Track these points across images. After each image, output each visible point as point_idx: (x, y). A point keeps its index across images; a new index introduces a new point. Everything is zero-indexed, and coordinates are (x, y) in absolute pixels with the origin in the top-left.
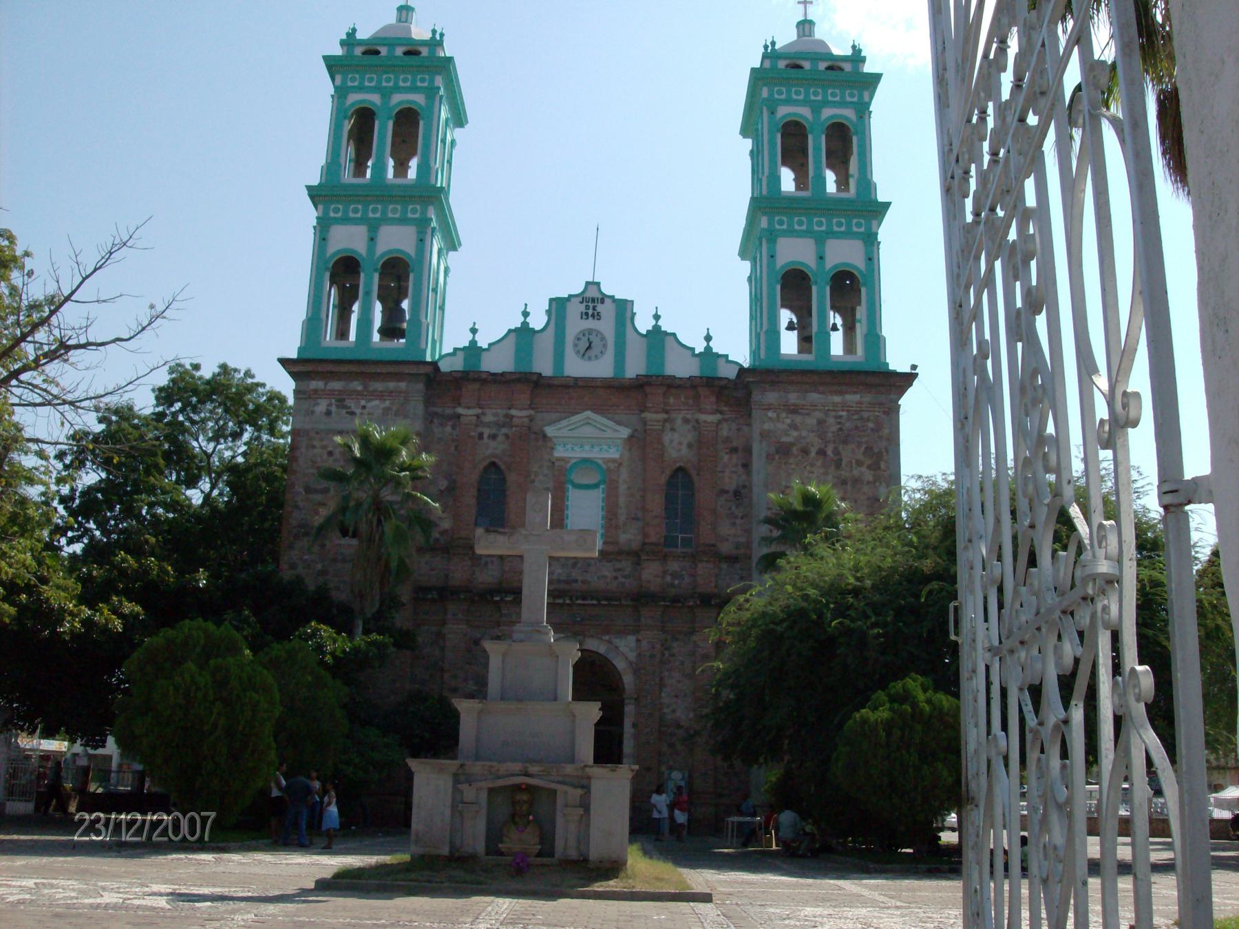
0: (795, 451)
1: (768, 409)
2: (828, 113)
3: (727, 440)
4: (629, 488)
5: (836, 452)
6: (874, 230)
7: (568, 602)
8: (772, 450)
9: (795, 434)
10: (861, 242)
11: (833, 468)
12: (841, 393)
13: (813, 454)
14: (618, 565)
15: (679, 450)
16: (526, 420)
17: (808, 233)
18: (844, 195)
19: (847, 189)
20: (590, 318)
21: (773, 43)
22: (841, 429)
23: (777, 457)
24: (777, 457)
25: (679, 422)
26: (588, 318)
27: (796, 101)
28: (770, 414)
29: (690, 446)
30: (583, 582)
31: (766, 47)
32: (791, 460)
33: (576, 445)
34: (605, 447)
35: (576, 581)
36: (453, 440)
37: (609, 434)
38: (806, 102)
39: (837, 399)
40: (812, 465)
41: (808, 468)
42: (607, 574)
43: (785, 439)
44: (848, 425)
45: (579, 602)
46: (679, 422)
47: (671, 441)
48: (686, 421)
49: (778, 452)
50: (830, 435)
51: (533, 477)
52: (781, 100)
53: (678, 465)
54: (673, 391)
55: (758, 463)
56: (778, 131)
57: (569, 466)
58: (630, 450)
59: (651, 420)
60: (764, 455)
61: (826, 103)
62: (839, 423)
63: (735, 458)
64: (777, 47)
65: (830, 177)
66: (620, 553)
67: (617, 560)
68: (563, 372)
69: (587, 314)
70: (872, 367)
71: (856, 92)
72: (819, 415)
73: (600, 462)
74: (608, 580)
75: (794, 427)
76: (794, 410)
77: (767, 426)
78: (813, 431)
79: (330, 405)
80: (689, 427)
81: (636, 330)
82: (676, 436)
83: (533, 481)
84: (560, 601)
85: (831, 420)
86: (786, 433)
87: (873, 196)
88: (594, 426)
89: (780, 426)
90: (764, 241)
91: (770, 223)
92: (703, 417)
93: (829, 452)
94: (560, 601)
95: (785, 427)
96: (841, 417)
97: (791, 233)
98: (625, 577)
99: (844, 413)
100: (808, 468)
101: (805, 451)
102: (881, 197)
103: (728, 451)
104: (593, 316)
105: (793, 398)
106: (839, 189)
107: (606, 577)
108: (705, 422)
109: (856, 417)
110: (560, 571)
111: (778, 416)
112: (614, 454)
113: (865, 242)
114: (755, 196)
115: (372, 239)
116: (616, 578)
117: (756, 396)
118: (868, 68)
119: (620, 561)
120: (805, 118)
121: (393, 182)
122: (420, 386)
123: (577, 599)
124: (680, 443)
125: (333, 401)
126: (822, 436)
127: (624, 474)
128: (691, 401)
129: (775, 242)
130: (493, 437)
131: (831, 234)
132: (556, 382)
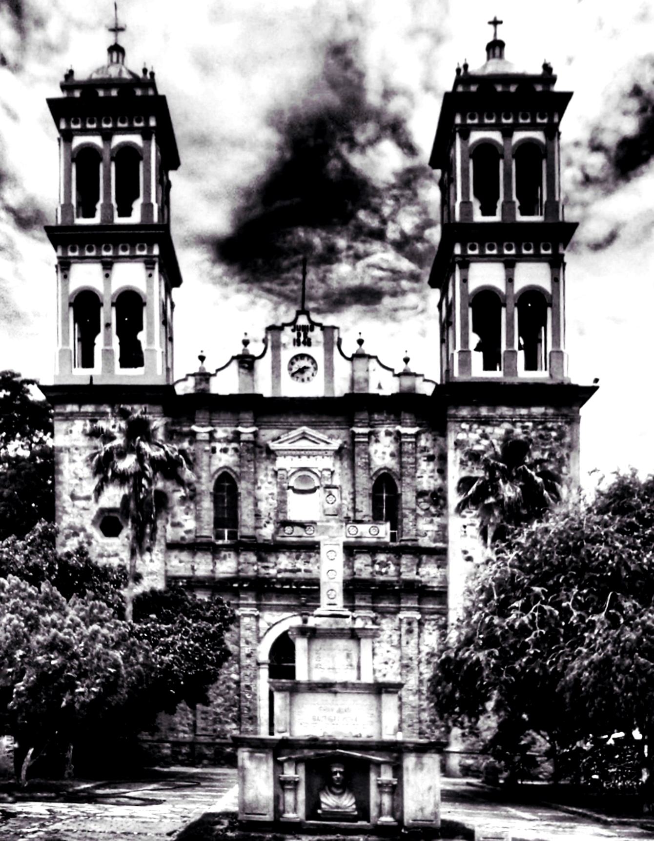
1: (462, 422)
30: (306, 571)
35: (299, 570)
37: (322, 446)
39: (524, 412)
43: (477, 448)
60: (458, 461)
75: (485, 436)
86: (478, 442)
88: (310, 440)
96: (527, 427)
99: (530, 424)
109: (540, 427)
118: (558, 88)
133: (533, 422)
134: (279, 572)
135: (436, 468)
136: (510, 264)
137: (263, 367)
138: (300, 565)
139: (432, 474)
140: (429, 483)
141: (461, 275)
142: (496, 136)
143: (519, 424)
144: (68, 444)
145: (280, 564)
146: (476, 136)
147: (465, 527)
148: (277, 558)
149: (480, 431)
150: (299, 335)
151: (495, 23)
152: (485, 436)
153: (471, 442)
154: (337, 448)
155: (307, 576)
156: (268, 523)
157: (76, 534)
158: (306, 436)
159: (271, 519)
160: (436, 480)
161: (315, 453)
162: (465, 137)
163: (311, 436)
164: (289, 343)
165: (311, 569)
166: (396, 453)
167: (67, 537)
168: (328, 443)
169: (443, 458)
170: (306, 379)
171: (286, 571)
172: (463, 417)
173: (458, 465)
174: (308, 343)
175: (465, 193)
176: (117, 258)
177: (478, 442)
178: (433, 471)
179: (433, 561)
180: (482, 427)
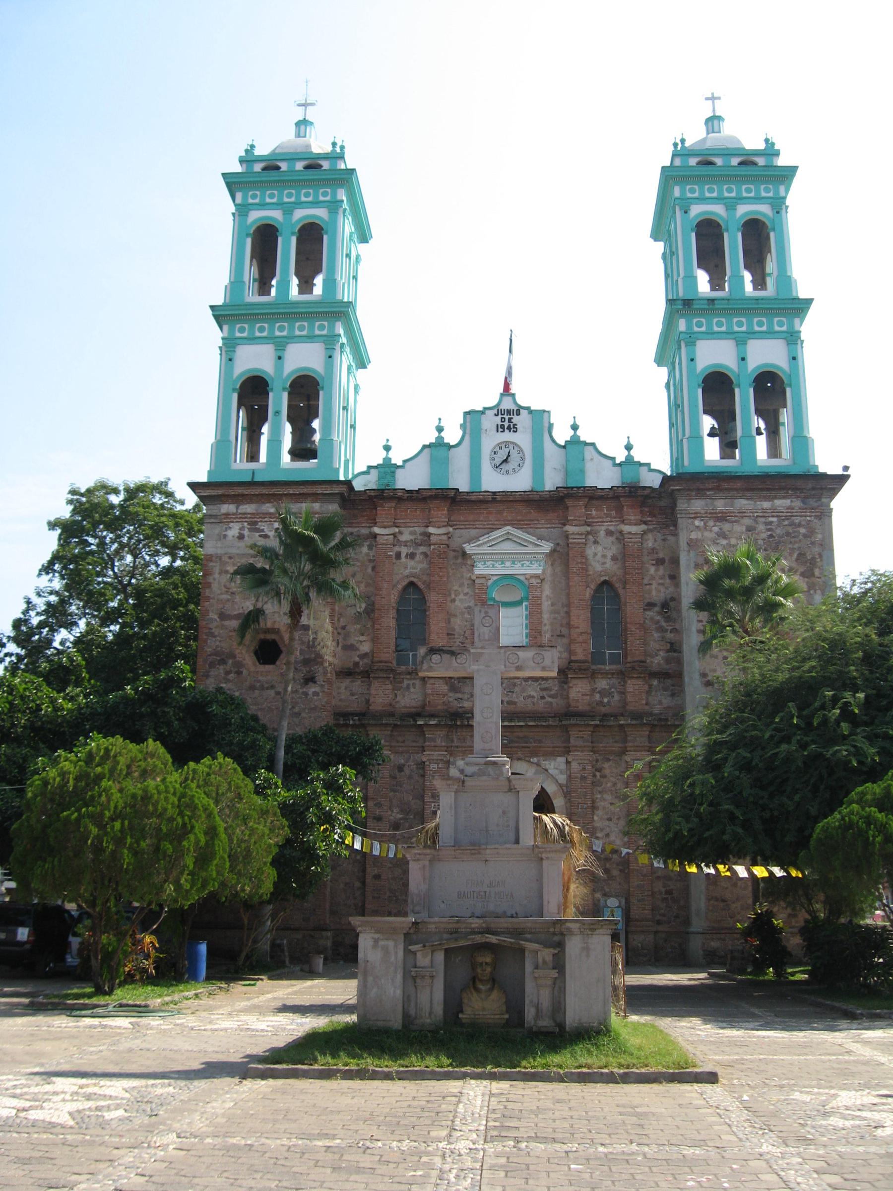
1: (695, 518)
3: (653, 550)
4: (552, 605)
16: (445, 538)
17: (729, 334)
21: (683, 141)
22: (771, 536)
25: (602, 533)
29: (614, 558)
36: (370, 561)
37: (530, 549)
38: (719, 199)
39: (766, 505)
47: (595, 554)
48: (609, 533)
51: (453, 596)
53: (602, 579)
58: (552, 565)
61: (740, 200)
62: (769, 530)
64: (687, 144)
65: (747, 277)
69: (503, 427)
72: (747, 521)
73: (522, 578)
76: (721, 518)
77: (693, 536)
79: (242, 529)
80: (611, 539)
81: (554, 441)
82: (600, 548)
83: (453, 601)
85: (761, 527)
89: (707, 534)
92: (626, 528)
95: (713, 535)
96: (771, 523)
98: (551, 696)
103: (654, 562)
105: (720, 505)
106: (713, 289)
107: (533, 697)
108: (630, 533)
109: (786, 523)
111: (705, 524)
112: (536, 569)
117: (682, 505)
124: (604, 556)
125: (246, 524)
127: (547, 591)
130: (412, 556)
132: (473, 498)
144: (220, 551)
149: (716, 529)
150: (503, 420)
151: (713, 98)
157: (223, 662)
160: (667, 588)
167: (212, 665)
170: (511, 471)
174: (513, 428)
178: (662, 578)
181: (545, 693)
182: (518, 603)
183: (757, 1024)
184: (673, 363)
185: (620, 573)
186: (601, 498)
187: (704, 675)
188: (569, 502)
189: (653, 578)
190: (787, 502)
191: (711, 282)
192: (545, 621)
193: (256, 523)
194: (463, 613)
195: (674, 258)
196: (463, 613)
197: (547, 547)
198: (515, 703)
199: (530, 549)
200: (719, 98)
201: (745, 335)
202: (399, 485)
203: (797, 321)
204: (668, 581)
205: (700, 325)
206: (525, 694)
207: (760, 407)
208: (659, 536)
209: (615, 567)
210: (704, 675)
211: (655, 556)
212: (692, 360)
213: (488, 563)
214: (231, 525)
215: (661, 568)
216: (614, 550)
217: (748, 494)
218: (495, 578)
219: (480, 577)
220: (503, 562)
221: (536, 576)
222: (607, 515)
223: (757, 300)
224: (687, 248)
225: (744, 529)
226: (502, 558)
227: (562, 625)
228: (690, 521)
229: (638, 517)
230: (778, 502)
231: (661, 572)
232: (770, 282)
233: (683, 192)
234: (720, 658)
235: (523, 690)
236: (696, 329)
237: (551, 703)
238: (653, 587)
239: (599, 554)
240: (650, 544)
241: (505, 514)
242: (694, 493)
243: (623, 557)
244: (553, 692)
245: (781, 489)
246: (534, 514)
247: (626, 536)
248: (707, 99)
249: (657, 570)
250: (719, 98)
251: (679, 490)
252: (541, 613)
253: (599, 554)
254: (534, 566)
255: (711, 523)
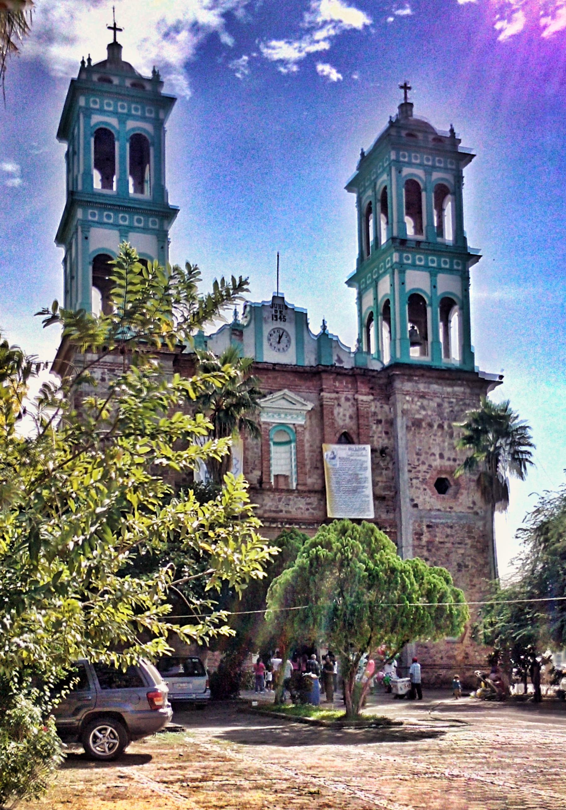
0: (424, 424)
1: (406, 395)
2: (131, 124)
3: (375, 414)
4: (311, 446)
5: (450, 427)
6: (165, 228)
7: (280, 526)
8: (410, 424)
9: (424, 413)
10: (154, 237)
11: (448, 437)
12: (452, 386)
13: (435, 427)
14: (308, 500)
15: (344, 420)
17: (426, 268)
18: (106, 191)
19: (142, 192)
20: (279, 320)
21: (89, 60)
22: (452, 411)
23: (413, 428)
24: (413, 428)
25: (343, 399)
26: (276, 320)
27: (414, 164)
28: (408, 398)
29: (351, 417)
30: (286, 512)
31: (83, 62)
32: (422, 431)
33: (275, 413)
34: (295, 416)
35: (281, 511)
37: (298, 406)
38: (115, 113)
39: (449, 389)
40: (435, 435)
41: (432, 437)
42: (301, 506)
43: (417, 416)
44: (456, 408)
45: (287, 526)
46: (343, 399)
47: (339, 414)
48: (347, 399)
49: (413, 424)
50: (445, 415)
52: (404, 162)
53: (344, 431)
54: (339, 377)
55: (401, 432)
56: (92, 135)
57: (271, 427)
58: (310, 418)
59: (326, 398)
60: (405, 426)
61: (129, 115)
62: (451, 407)
63: (380, 428)
64: (93, 63)
65: (97, 176)
66: (310, 492)
67: (308, 497)
68: (262, 358)
69: (276, 316)
70: (466, 368)
71: (126, 104)
72: (438, 400)
73: (291, 426)
74: (303, 511)
75: (423, 407)
76: (423, 396)
77: (405, 407)
78: (435, 412)
79: (103, 373)
80: (349, 403)
82: (341, 410)
84: (274, 525)
85: (446, 405)
86: (418, 412)
87: (166, 201)
88: (287, 400)
89: (413, 406)
90: (396, 272)
91: (401, 257)
92: (360, 397)
93: (446, 427)
94: (274, 525)
95: (417, 407)
96: (452, 402)
97: (414, 266)
98: (313, 509)
99: (454, 400)
100: (432, 437)
101: (430, 425)
102: (171, 202)
104: (280, 318)
105: (422, 387)
106: (103, 187)
107: (301, 509)
108: (362, 401)
109: (461, 403)
110: (270, 504)
111: (412, 400)
112: (301, 421)
113: (158, 238)
114: (71, 189)
115: (162, 248)
116: (308, 509)
117: (398, 384)
118: (165, 91)
119: (310, 497)
120: (113, 127)
121: (100, 192)
122: (171, 363)
123: (286, 524)
124: (344, 415)
125: (106, 370)
126: (440, 414)
127: (307, 437)
128: (350, 386)
129: (404, 272)
131: (440, 269)
133: (456, 398)
134: (265, 512)
135: (384, 430)
136: (433, 273)
137: (249, 336)
138: (281, 506)
139: (380, 435)
140: (378, 442)
141: (400, 278)
142: (113, 121)
143: (446, 400)
145: (266, 505)
146: (96, 119)
147: (411, 479)
148: (263, 500)
149: (419, 403)
150: (276, 311)
151: (115, 29)
152: (423, 407)
153: (413, 412)
154: (310, 409)
155: (288, 516)
156: (254, 469)
158: (285, 397)
159: (256, 466)
160: (383, 440)
161: (291, 411)
162: (88, 117)
163: (290, 397)
164: (268, 318)
165: (291, 510)
166: (354, 416)
168: (304, 405)
169: (391, 423)
170: (281, 350)
171: (270, 511)
172: (407, 391)
173: (405, 430)
175: (123, 172)
176: (131, 228)
177: (418, 412)
178: (381, 432)
179: (383, 506)
180: (421, 400)
181: (309, 507)
182: (288, 443)
183: (219, 730)
184: (71, 244)
185: (355, 427)
186: (345, 375)
187: (412, 500)
188: (324, 376)
189: (375, 433)
190: (462, 389)
191: (102, 180)
192: (306, 457)
193: (113, 370)
194: (252, 448)
195: (76, 157)
196: (252, 448)
197: (310, 406)
198: (290, 512)
199: (298, 406)
200: (120, 30)
201: (126, 228)
202: (265, 360)
203: (166, 222)
204: (384, 435)
205: (93, 215)
206: (296, 506)
207: (412, 318)
208: (378, 404)
209: (352, 423)
210: (412, 500)
211: (376, 418)
212: (403, 284)
213: (270, 414)
214: (95, 370)
215: (380, 426)
216: (351, 411)
217: (440, 381)
218: (274, 425)
219: (265, 423)
220: (279, 415)
221: (301, 426)
222: (347, 387)
223: (135, 200)
224: (87, 149)
225: (436, 405)
226: (279, 411)
227: (317, 460)
228: (403, 396)
229: (367, 390)
230: (456, 389)
231: (380, 429)
232: (147, 188)
233: (87, 102)
234: (422, 489)
235: (295, 503)
236: (90, 218)
237: (313, 514)
238: (375, 438)
239: (341, 414)
240: (373, 409)
241: (279, 380)
242: (406, 378)
243: (358, 415)
244: (314, 506)
245: (459, 379)
246: (297, 382)
247: (359, 402)
248: (109, 28)
249: (377, 428)
250: (120, 30)
251: (397, 375)
252: (304, 451)
253: (341, 414)
254: (300, 418)
255: (416, 399)
